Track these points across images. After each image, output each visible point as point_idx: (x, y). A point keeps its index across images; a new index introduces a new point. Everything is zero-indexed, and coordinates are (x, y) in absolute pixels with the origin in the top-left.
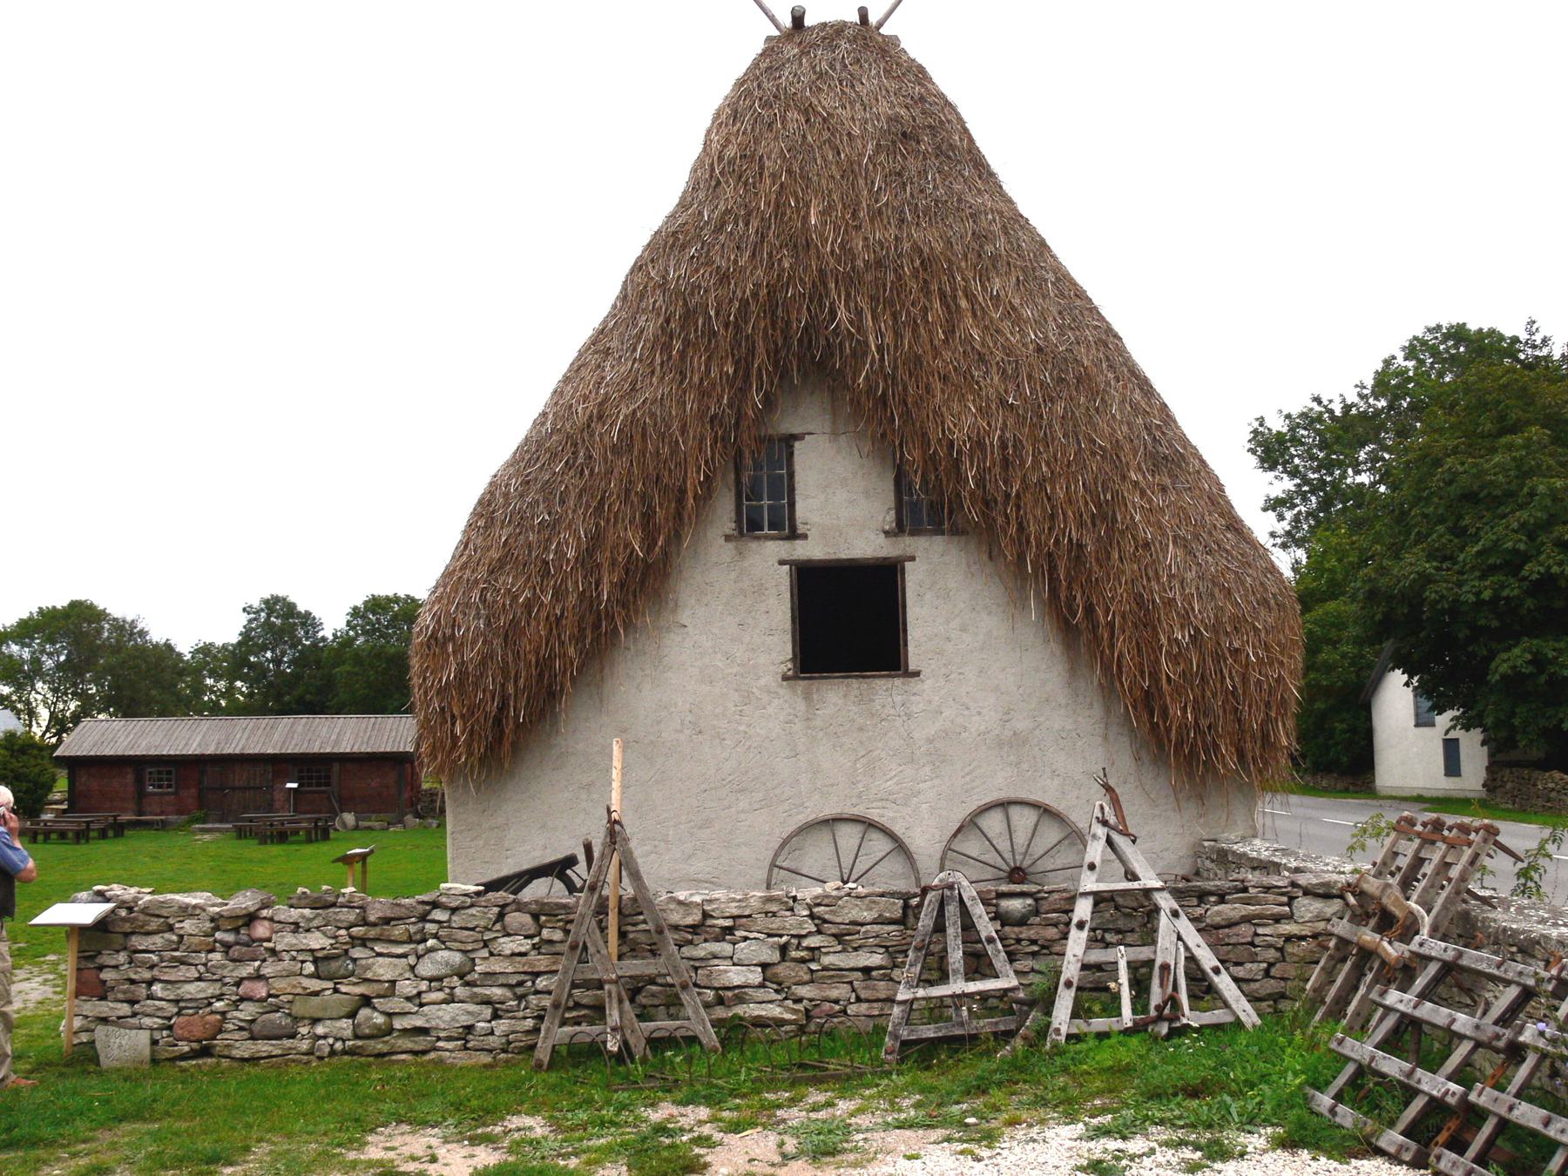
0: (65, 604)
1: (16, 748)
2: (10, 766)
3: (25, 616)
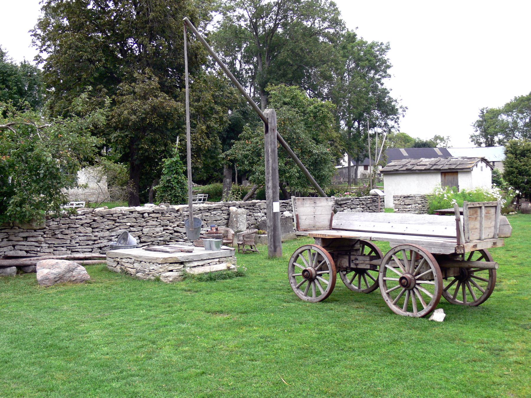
0: (528, 94)
1: (518, 152)
2: (515, 165)
3: (509, 102)
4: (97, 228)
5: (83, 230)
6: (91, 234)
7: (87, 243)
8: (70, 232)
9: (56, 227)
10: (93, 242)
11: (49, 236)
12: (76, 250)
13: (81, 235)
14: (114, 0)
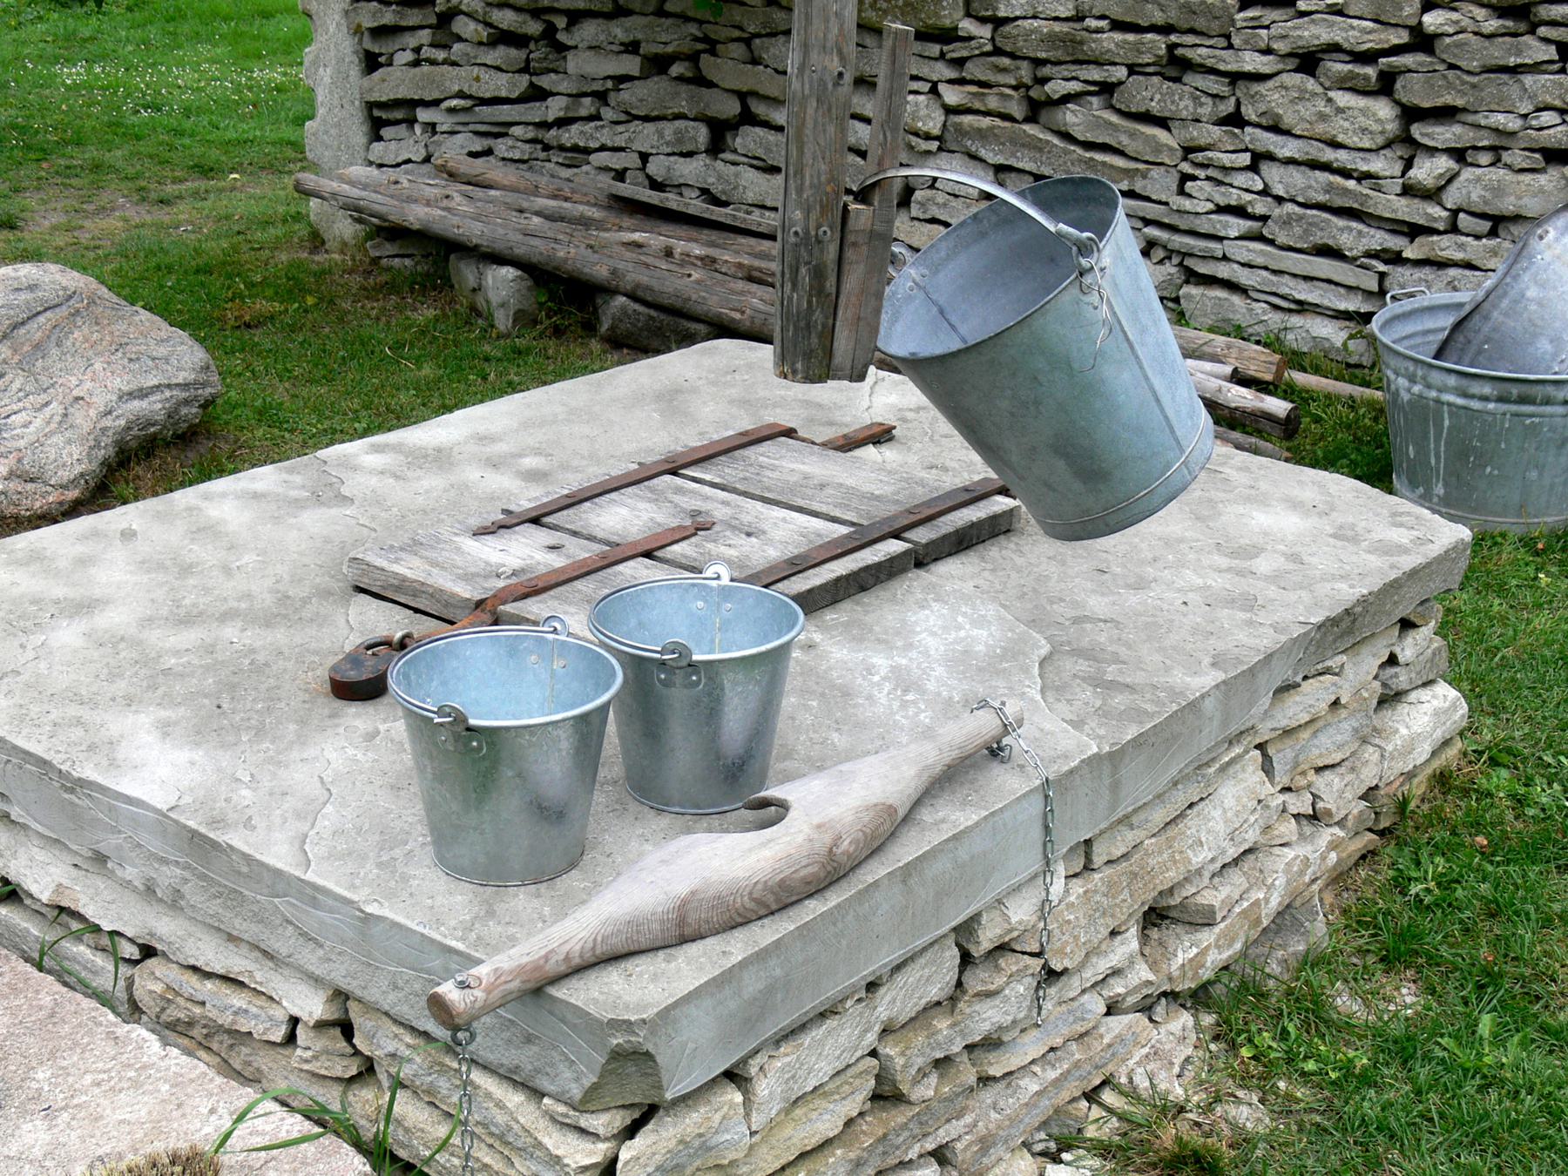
4: (1446, 114)
5: (1307, 110)
6: (1377, 165)
7: (1320, 238)
8: (1185, 107)
9: (1052, 40)
10: (1379, 239)
11: (993, 103)
12: (1223, 271)
13: (1287, 148)
14: (96, 0)
